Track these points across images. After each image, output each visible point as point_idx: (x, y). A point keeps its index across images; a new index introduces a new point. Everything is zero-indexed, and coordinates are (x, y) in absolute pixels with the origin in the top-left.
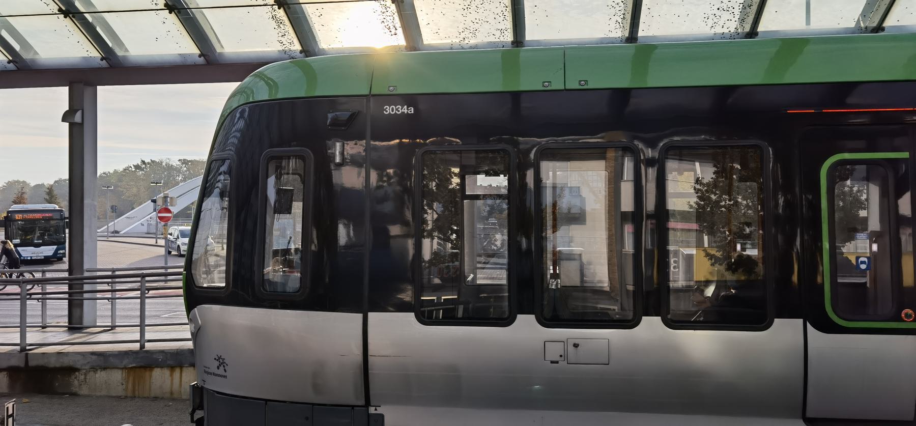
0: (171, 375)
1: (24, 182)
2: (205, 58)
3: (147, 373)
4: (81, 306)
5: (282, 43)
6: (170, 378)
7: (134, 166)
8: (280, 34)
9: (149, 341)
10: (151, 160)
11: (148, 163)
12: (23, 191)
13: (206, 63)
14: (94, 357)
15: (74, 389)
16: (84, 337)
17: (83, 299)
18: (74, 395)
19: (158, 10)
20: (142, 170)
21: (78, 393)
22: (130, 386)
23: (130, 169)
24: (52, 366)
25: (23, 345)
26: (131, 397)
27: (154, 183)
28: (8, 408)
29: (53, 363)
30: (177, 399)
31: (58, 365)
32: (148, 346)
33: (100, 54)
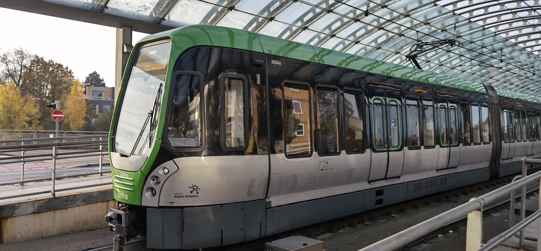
32: (57, 194)
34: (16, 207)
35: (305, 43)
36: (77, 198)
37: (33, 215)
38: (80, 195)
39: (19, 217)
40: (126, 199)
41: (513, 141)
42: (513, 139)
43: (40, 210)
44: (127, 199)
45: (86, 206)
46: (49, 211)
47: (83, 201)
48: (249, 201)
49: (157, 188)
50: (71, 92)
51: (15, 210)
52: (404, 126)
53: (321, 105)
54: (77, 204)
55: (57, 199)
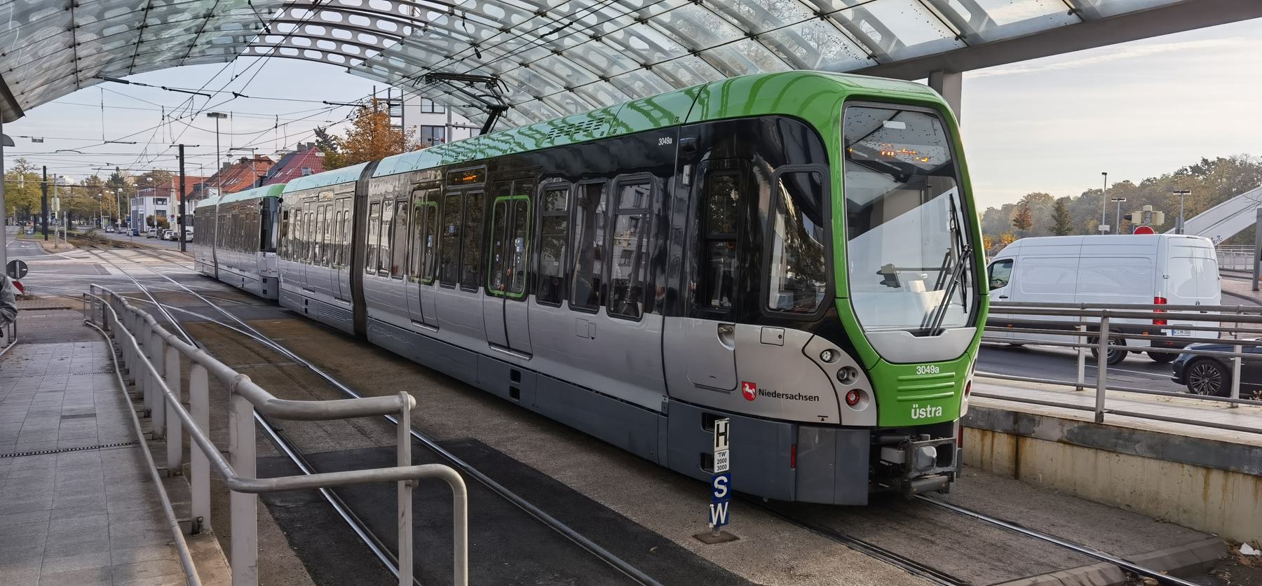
0: (982, 440)
1: (1046, 195)
2: (1078, 15)
7: (1191, 168)
9: (1110, 412)
10: (1218, 158)
11: (1213, 163)
12: (1027, 207)
13: (1081, 21)
20: (1204, 173)
23: (1185, 172)
27: (1178, 192)
28: (718, 425)
32: (1108, 418)
33: (1068, 5)
34: (1036, 422)
37: (1061, 444)
39: (1041, 441)
40: (929, 416)
41: (520, 296)
42: (523, 289)
44: (940, 414)
45: (1158, 462)
46: (1087, 447)
47: (1148, 448)
48: (616, 398)
49: (843, 389)
50: (1234, 161)
52: (471, 181)
54: (1138, 450)
55: (1099, 428)
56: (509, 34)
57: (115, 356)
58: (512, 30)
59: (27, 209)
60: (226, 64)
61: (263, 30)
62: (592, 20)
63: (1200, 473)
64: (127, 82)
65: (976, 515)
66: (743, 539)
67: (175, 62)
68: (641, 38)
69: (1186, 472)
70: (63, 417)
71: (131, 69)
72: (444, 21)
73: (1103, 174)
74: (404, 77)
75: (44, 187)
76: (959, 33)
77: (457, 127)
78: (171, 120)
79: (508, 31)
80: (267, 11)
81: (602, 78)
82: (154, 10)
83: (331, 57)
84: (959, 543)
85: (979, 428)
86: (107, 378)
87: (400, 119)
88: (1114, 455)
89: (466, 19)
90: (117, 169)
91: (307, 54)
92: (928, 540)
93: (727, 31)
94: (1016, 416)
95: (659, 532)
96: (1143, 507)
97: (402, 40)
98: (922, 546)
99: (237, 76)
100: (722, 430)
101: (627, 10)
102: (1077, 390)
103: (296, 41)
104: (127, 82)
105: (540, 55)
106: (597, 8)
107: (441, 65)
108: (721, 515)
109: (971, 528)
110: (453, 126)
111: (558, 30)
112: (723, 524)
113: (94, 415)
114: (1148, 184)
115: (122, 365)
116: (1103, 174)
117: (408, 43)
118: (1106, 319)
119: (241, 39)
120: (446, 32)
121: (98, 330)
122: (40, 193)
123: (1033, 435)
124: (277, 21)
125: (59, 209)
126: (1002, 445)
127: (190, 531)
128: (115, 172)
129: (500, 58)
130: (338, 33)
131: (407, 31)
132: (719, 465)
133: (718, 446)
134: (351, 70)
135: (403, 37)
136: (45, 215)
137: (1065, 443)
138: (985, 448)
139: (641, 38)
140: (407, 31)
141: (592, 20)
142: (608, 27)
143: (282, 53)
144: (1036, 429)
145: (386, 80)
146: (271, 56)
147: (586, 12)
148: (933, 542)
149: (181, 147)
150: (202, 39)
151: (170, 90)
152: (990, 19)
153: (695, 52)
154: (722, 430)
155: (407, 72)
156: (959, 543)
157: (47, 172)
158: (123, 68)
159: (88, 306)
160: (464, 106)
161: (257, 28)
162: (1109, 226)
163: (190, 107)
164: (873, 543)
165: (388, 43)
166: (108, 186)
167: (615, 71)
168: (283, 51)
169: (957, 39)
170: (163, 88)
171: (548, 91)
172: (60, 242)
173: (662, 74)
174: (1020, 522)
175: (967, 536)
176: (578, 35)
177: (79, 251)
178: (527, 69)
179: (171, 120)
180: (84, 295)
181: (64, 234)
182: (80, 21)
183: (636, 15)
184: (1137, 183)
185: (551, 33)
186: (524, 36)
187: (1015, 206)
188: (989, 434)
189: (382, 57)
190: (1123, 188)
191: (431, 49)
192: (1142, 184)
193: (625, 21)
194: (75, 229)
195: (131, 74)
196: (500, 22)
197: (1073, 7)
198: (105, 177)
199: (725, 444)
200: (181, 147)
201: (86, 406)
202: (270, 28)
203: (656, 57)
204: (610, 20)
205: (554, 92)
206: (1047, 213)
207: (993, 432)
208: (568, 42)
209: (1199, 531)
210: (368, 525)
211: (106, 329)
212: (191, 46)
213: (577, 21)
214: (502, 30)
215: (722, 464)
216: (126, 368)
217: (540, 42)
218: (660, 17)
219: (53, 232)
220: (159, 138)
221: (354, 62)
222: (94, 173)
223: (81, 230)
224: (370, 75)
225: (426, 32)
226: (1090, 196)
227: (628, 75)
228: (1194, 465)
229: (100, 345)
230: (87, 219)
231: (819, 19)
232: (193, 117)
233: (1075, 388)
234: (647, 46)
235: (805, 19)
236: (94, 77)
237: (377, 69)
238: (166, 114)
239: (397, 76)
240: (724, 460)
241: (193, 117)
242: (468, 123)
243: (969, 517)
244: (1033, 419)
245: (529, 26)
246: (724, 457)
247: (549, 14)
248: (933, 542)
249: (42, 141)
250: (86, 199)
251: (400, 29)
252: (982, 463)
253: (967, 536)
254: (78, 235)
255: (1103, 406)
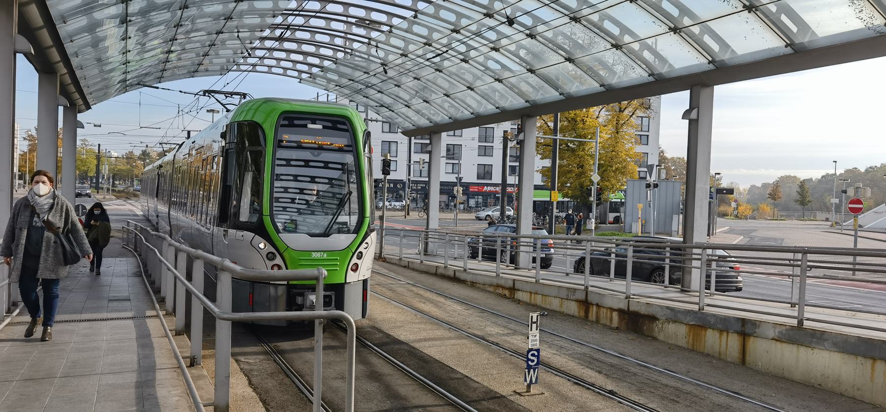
0: (720, 337)
3: (703, 332)
4: (690, 273)
5: (862, 19)
6: (719, 340)
8: (857, 11)
9: (808, 319)
12: (778, 185)
14: (668, 311)
15: (656, 334)
16: (686, 297)
17: (692, 268)
18: (655, 339)
19: (739, 12)
21: (658, 337)
22: (691, 340)
24: (643, 313)
25: (629, 294)
26: (691, 350)
28: (532, 317)
29: (643, 310)
30: (723, 360)
31: (646, 313)
32: (807, 324)
34: (757, 326)
35: (78, 119)
36: (825, 336)
38: (830, 333)
39: (760, 339)
43: (780, 338)
51: (756, 328)
53: (391, 196)
54: (826, 346)
56: (407, 58)
57: (142, 267)
58: (409, 55)
59: (86, 172)
60: (221, 76)
61: (246, 54)
62: (462, 48)
63: (869, 362)
64: (158, 88)
65: (711, 387)
66: (547, 394)
67: (188, 75)
68: (497, 62)
69: (859, 361)
70: (110, 300)
71: (160, 79)
72: (364, 48)
73: (834, 161)
74: (336, 86)
75: (98, 158)
76: (710, 59)
77: (372, 121)
78: (184, 113)
79: (406, 56)
80: (249, 42)
81: (469, 88)
82: (178, 41)
83: (289, 72)
84: (696, 403)
85: (718, 329)
86: (137, 280)
87: (698, 298)
88: (810, 349)
89: (379, 47)
90: (147, 146)
91: (274, 70)
92: (675, 400)
93: (555, 58)
94: (744, 321)
95: (492, 388)
96: (830, 386)
97: (336, 61)
98: (670, 404)
99: (228, 84)
100: (534, 320)
101: (486, 42)
102: (791, 307)
103: (266, 62)
104: (158, 88)
105: (428, 73)
106: (465, 40)
107: (361, 78)
108: (533, 377)
109: (706, 395)
110: (369, 120)
111: (439, 55)
112: (534, 384)
113: (129, 300)
114: (871, 170)
115: (146, 272)
116: (834, 161)
117: (340, 63)
118: (805, 255)
119: (232, 60)
120: (366, 57)
121: (131, 251)
122: (95, 162)
123: (755, 335)
124: (255, 48)
125: (107, 173)
126: (733, 342)
127: (189, 365)
128: (144, 149)
129: (401, 74)
130: (294, 57)
131: (340, 55)
132: (532, 343)
133: (531, 330)
134: (302, 81)
135: (337, 59)
136: (97, 178)
137: (777, 340)
138: (722, 344)
139: (497, 62)
140: (340, 55)
141: (462, 48)
142: (473, 53)
143: (242, 69)
144: (757, 330)
145: (324, 88)
146: (250, 71)
147: (458, 43)
148: (677, 402)
149: (189, 132)
150: (206, 61)
151: (185, 93)
152: (732, 49)
153: (531, 71)
154: (534, 320)
155: (339, 83)
156: (696, 403)
157: (101, 148)
158: (155, 79)
159: (125, 236)
160: (376, 106)
161: (242, 53)
162: (838, 200)
163: (197, 105)
164: (636, 400)
165: (326, 63)
166: (139, 158)
167: (478, 83)
168: (258, 68)
169: (709, 63)
170: (180, 91)
171: (434, 96)
172: (107, 195)
173: (512, 87)
174: (742, 392)
175: (702, 399)
176: (452, 58)
177: (118, 201)
178: (419, 81)
179: (184, 113)
180: (123, 227)
181: (109, 190)
182: (130, 47)
183: (492, 45)
184: (863, 170)
185: (434, 57)
186: (415, 57)
187: (771, 184)
188: (725, 334)
189: (323, 73)
190: (852, 174)
191: (356, 68)
192: (866, 170)
193: (485, 49)
194: (116, 187)
195: (160, 82)
196: (402, 50)
197: (789, 42)
198: (137, 152)
199: (537, 330)
200: (189, 132)
201: (125, 294)
202: (250, 52)
203: (507, 74)
204: (475, 49)
205: (437, 98)
206: (795, 190)
207: (728, 333)
208: (446, 63)
209: (868, 403)
210: (300, 376)
211: (136, 251)
212: (200, 64)
213: (452, 49)
214: (402, 55)
215: (534, 343)
216: (149, 273)
217: (427, 63)
218: (508, 47)
219: (102, 188)
220: (175, 125)
221: (304, 76)
222: (131, 149)
223: (120, 188)
224: (315, 85)
225: (352, 56)
226: (827, 179)
227: (486, 87)
228: (865, 357)
229: (132, 260)
230: (125, 181)
231: (615, 49)
232: (198, 111)
233: (790, 305)
234: (499, 67)
235: (605, 49)
236: (136, 84)
237: (319, 80)
238: (180, 110)
239: (332, 86)
240: (536, 340)
241: (198, 111)
242: (380, 118)
243: (706, 388)
244: (755, 324)
245: (420, 52)
246: (535, 338)
247: (433, 44)
248: (677, 402)
249: (100, 126)
250: (123, 167)
251: (335, 53)
252: (720, 354)
253: (702, 399)
254: (118, 190)
255: (803, 315)
